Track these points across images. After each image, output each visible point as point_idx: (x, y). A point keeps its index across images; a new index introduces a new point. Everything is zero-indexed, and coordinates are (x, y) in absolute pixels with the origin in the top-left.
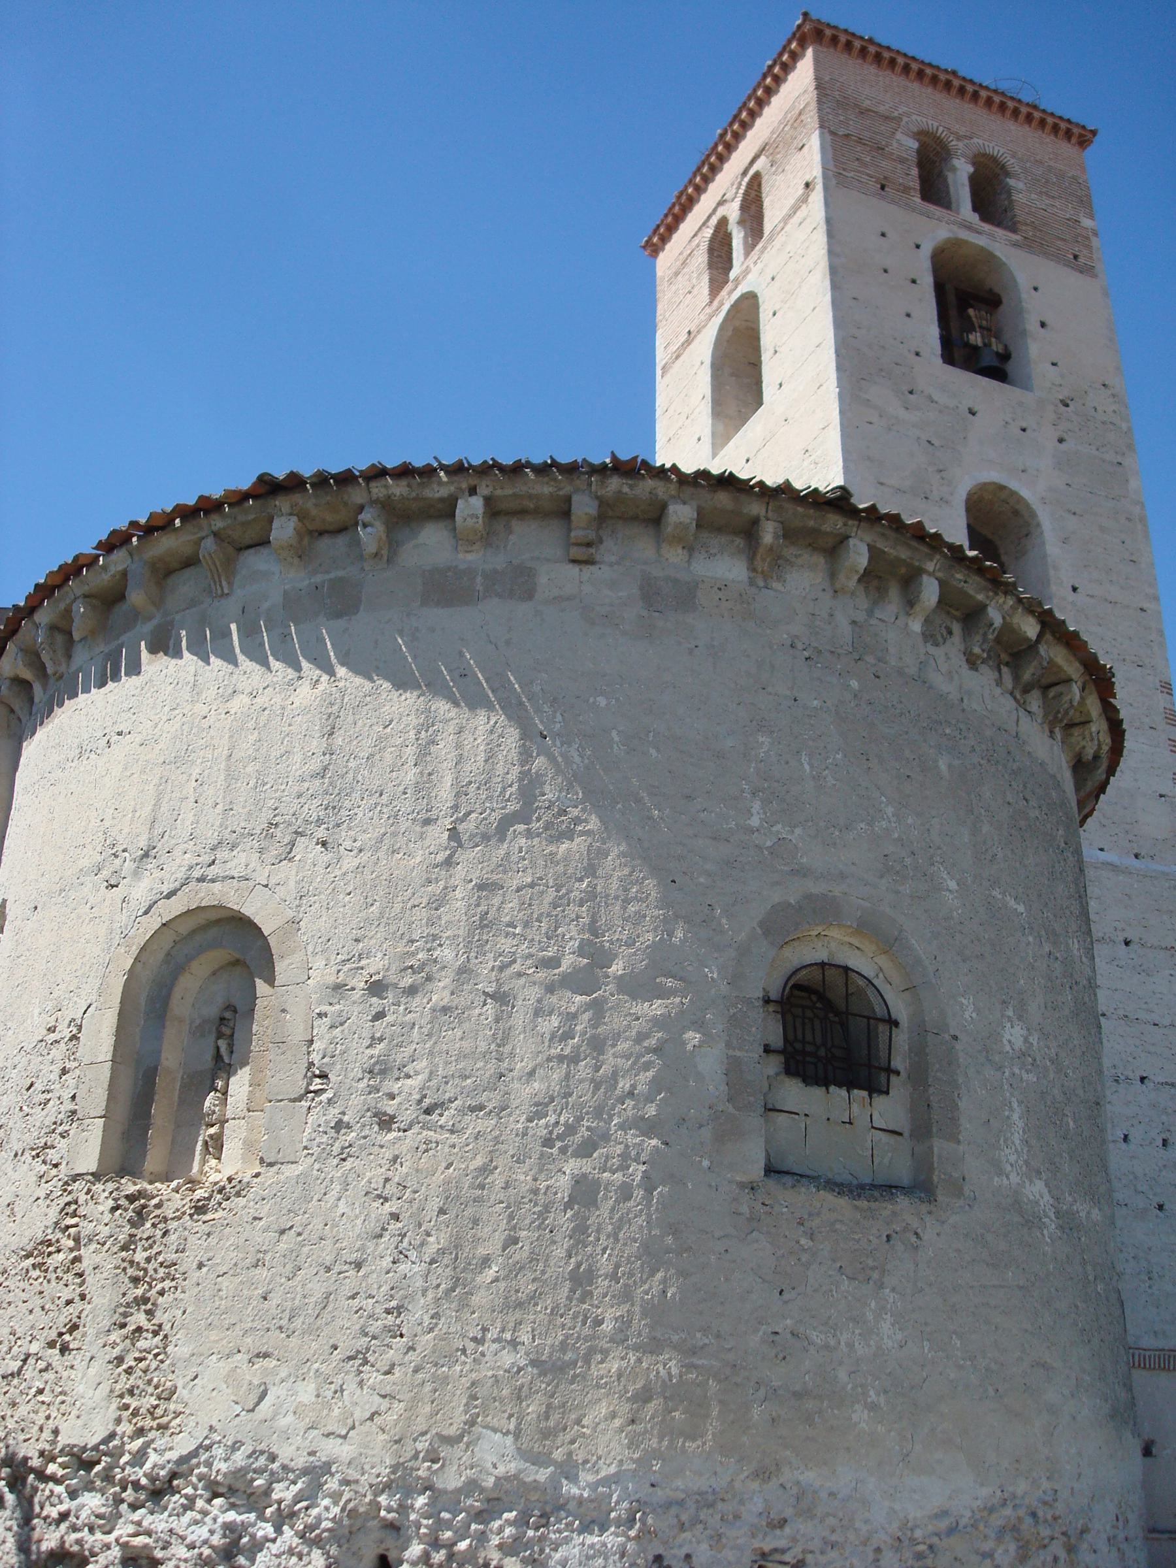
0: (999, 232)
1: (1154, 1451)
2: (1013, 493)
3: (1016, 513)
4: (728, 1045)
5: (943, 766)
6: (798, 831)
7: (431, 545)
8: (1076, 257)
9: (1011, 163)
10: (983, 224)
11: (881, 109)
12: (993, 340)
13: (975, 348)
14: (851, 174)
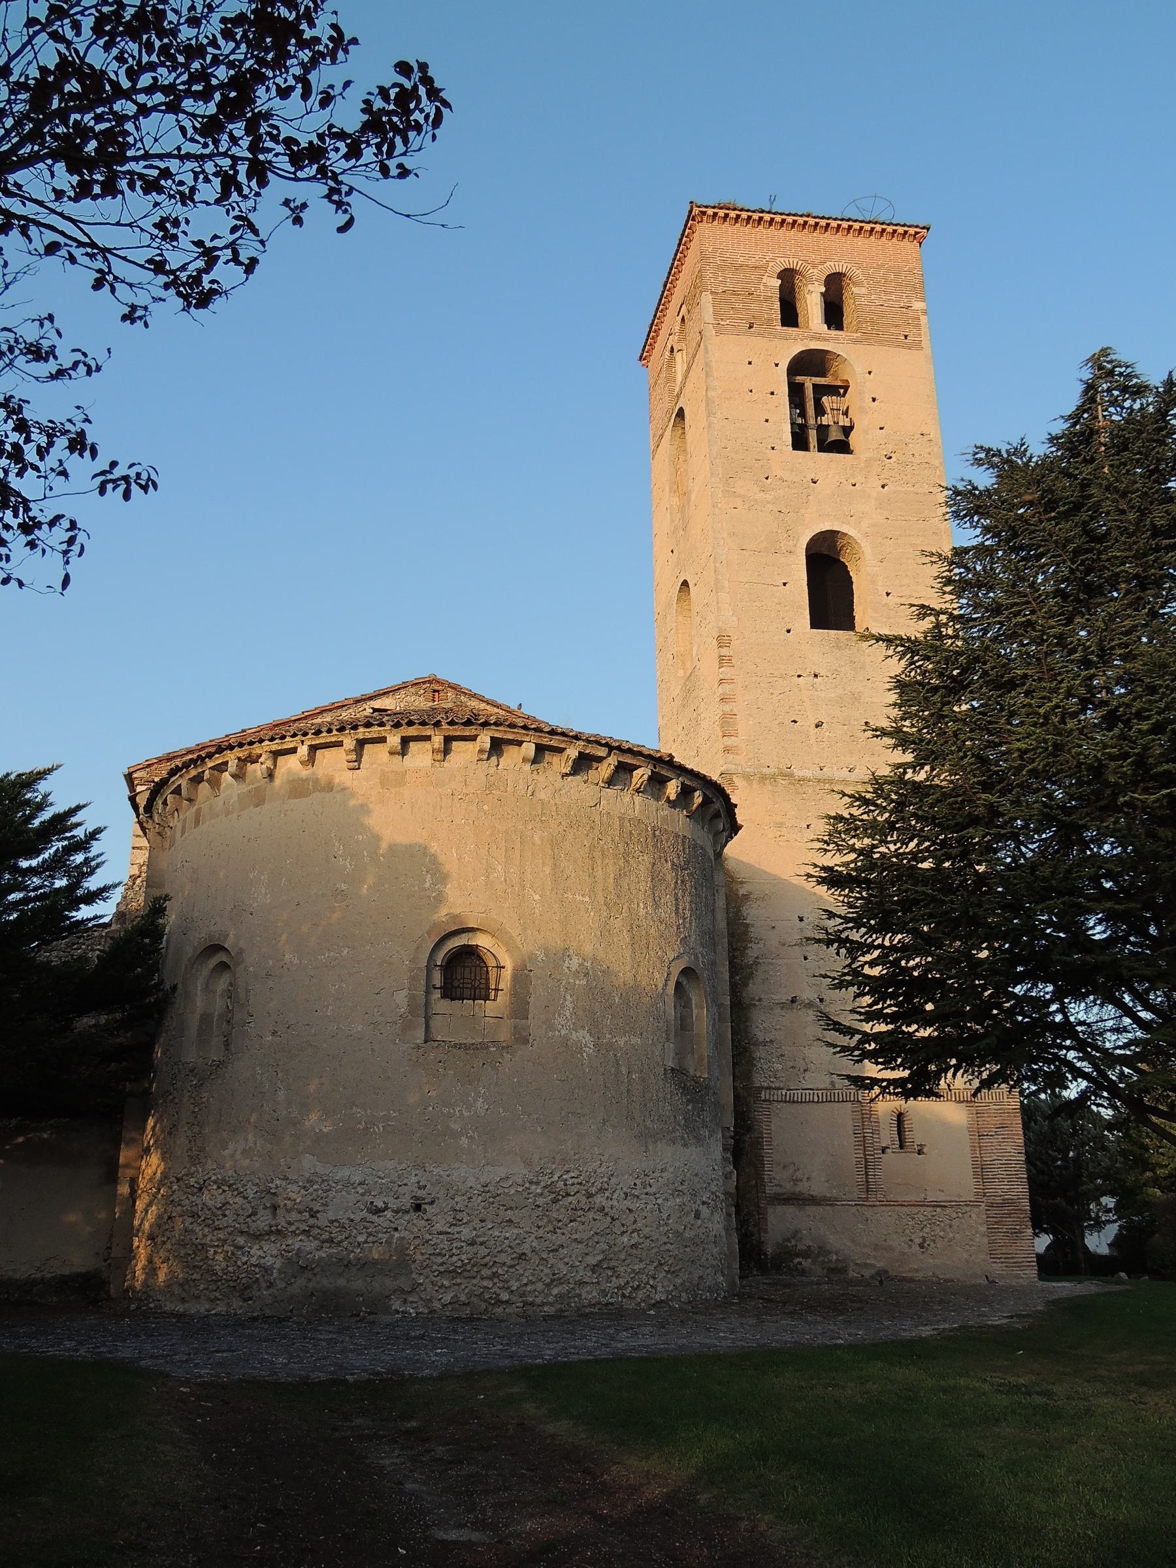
8: (906, 337)
9: (857, 273)
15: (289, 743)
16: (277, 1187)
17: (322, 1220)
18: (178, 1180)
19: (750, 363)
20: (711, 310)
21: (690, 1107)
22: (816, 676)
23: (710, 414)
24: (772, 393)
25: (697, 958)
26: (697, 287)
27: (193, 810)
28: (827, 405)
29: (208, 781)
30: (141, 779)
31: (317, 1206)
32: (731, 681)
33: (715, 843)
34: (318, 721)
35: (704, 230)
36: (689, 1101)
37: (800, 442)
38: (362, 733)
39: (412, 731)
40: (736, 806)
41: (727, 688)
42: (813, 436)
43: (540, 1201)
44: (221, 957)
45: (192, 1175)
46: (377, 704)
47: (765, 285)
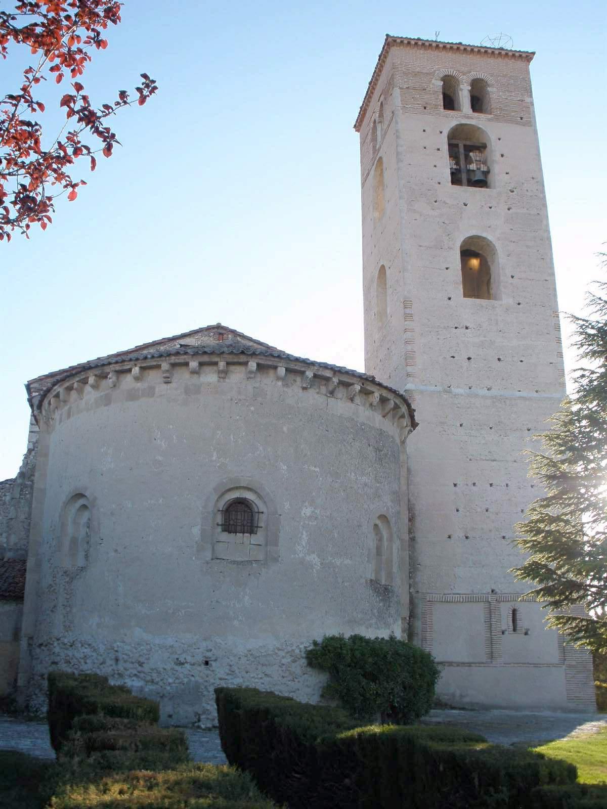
0: (482, 116)
1: (529, 632)
2: (485, 238)
3: (488, 245)
4: (202, 526)
5: (285, 429)
6: (228, 460)
7: (128, 381)
8: (522, 118)
9: (490, 80)
10: (474, 114)
11: (425, 71)
12: (482, 165)
13: (473, 171)
14: (410, 106)
15: (127, 366)
16: (118, 647)
17: (146, 668)
18: (58, 640)
19: (424, 131)
20: (400, 98)
21: (381, 604)
22: (467, 328)
23: (399, 161)
24: (438, 149)
25: (388, 509)
26: (390, 84)
27: (66, 408)
28: (473, 157)
29: (76, 389)
30: (35, 388)
31: (142, 660)
32: (412, 330)
33: (400, 435)
34: (145, 352)
35: (394, 50)
36: (381, 600)
37: (456, 179)
38: (173, 359)
39: (206, 359)
40: (414, 410)
41: (409, 334)
42: (464, 177)
43: (284, 661)
44: (81, 502)
45: (65, 637)
46: (183, 342)
47: (433, 84)
